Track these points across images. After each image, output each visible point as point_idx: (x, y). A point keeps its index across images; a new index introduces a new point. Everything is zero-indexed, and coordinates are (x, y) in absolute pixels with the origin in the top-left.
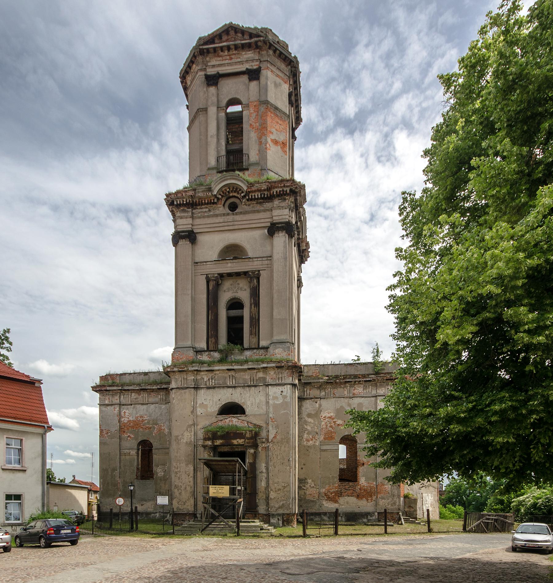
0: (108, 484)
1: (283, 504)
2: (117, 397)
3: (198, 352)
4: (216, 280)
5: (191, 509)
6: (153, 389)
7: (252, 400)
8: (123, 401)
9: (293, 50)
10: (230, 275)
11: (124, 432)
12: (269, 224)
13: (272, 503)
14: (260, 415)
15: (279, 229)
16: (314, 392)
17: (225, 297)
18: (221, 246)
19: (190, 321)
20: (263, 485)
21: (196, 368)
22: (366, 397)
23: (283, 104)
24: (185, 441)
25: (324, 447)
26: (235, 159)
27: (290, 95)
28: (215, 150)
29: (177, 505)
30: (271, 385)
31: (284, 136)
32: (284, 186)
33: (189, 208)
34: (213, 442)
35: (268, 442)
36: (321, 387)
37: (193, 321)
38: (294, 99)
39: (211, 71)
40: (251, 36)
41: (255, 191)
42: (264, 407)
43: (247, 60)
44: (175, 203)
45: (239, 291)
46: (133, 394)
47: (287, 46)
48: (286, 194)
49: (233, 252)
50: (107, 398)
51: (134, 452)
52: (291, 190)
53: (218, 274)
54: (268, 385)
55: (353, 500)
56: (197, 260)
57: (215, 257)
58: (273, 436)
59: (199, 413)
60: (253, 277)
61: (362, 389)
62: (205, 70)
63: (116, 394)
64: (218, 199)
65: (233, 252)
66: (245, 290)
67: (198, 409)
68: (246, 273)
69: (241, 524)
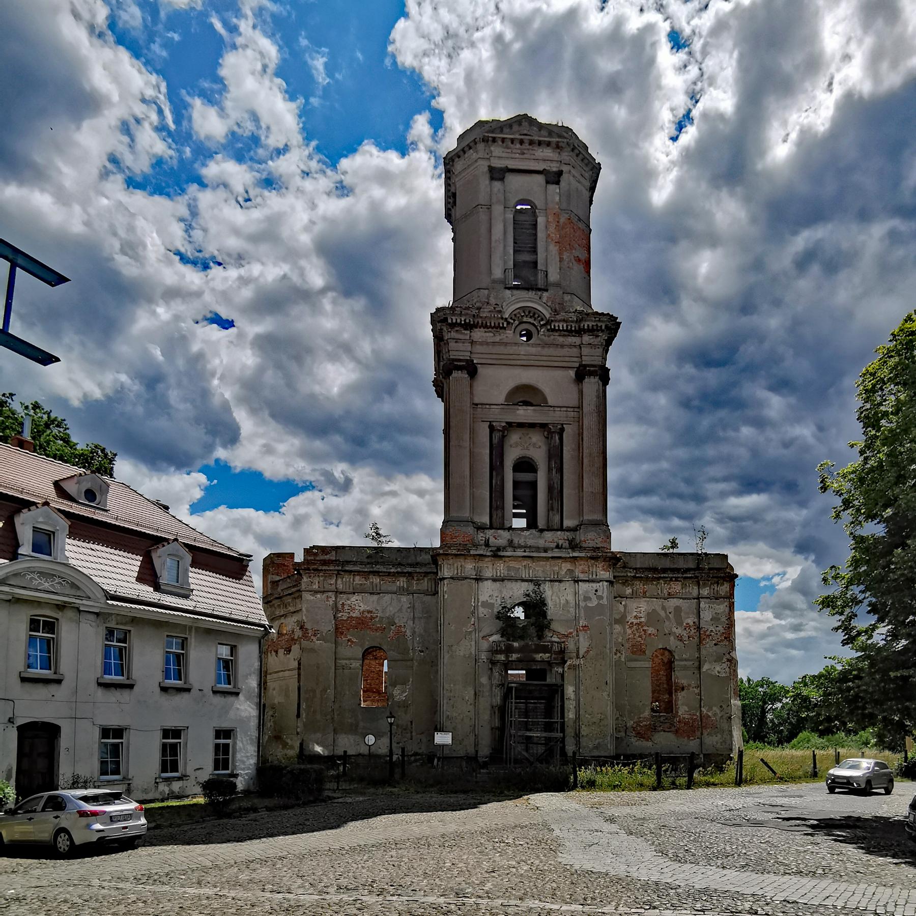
0: (315, 712)
1: (599, 743)
2: (333, 582)
6: (390, 573)
7: (559, 599)
8: (340, 586)
10: (521, 425)
11: (342, 633)
12: (577, 365)
13: (584, 742)
14: (567, 621)
15: (591, 374)
17: (511, 456)
18: (511, 385)
19: (467, 483)
20: (571, 716)
21: (481, 552)
22: (684, 599)
24: (462, 654)
30: (581, 581)
32: (599, 321)
33: (466, 329)
34: (507, 657)
35: (578, 657)
37: (472, 485)
41: (560, 321)
42: (572, 610)
44: (450, 321)
45: (531, 448)
46: (357, 578)
49: (525, 395)
50: (316, 580)
51: (358, 665)
53: (507, 423)
54: (577, 581)
55: (671, 736)
56: (476, 401)
57: (501, 399)
58: (586, 649)
61: (680, 588)
63: (330, 576)
64: (508, 323)
66: (540, 447)
67: (481, 609)
68: (543, 426)
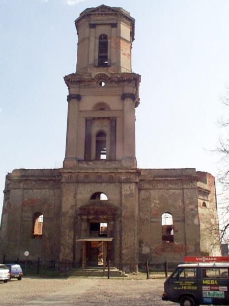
3: (79, 161)
4: (91, 121)
5: (71, 260)
9: (132, 15)
16: (147, 186)
23: (128, 38)
24: (69, 215)
25: (153, 220)
26: (103, 60)
27: (131, 32)
28: (94, 55)
29: (62, 257)
31: (128, 52)
36: (150, 182)
38: (132, 34)
39: (92, 22)
40: (113, 10)
43: (112, 19)
47: (129, 14)
48: (131, 80)
49: (101, 107)
52: (134, 79)
56: (81, 109)
59: (78, 198)
60: (113, 121)
62: (90, 21)
64: (94, 80)
65: (101, 107)
67: (78, 195)
69: (110, 270)
